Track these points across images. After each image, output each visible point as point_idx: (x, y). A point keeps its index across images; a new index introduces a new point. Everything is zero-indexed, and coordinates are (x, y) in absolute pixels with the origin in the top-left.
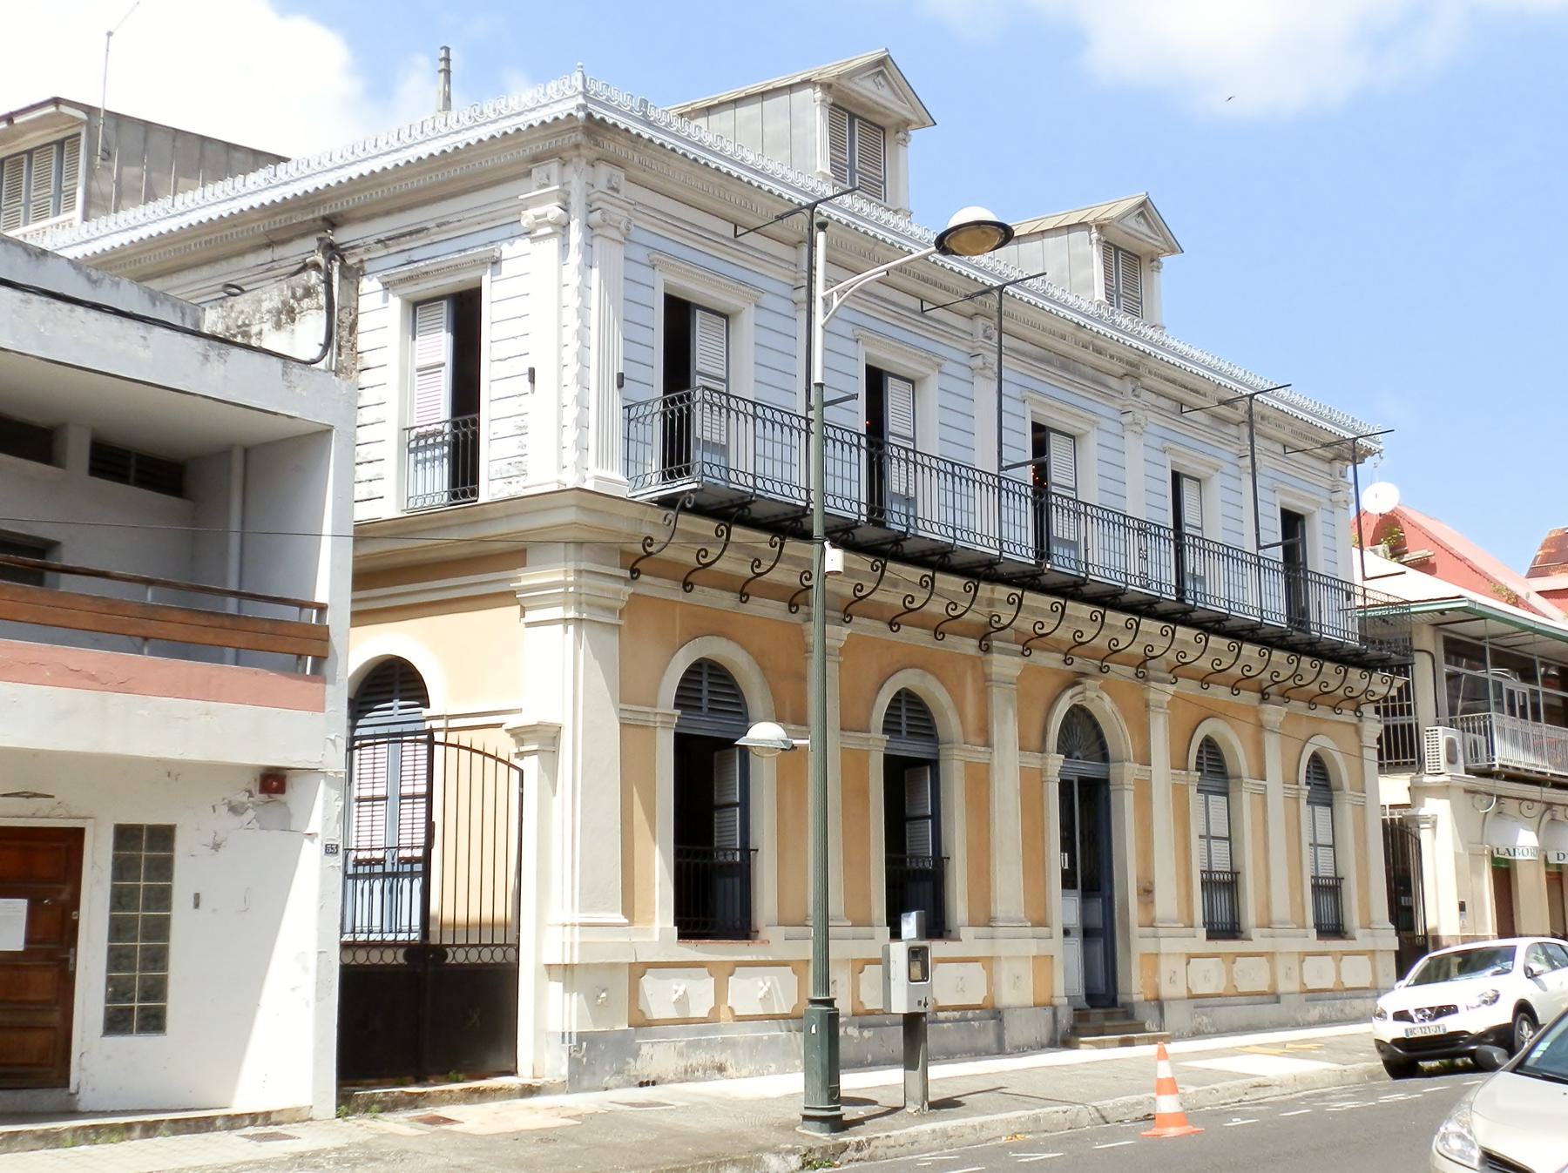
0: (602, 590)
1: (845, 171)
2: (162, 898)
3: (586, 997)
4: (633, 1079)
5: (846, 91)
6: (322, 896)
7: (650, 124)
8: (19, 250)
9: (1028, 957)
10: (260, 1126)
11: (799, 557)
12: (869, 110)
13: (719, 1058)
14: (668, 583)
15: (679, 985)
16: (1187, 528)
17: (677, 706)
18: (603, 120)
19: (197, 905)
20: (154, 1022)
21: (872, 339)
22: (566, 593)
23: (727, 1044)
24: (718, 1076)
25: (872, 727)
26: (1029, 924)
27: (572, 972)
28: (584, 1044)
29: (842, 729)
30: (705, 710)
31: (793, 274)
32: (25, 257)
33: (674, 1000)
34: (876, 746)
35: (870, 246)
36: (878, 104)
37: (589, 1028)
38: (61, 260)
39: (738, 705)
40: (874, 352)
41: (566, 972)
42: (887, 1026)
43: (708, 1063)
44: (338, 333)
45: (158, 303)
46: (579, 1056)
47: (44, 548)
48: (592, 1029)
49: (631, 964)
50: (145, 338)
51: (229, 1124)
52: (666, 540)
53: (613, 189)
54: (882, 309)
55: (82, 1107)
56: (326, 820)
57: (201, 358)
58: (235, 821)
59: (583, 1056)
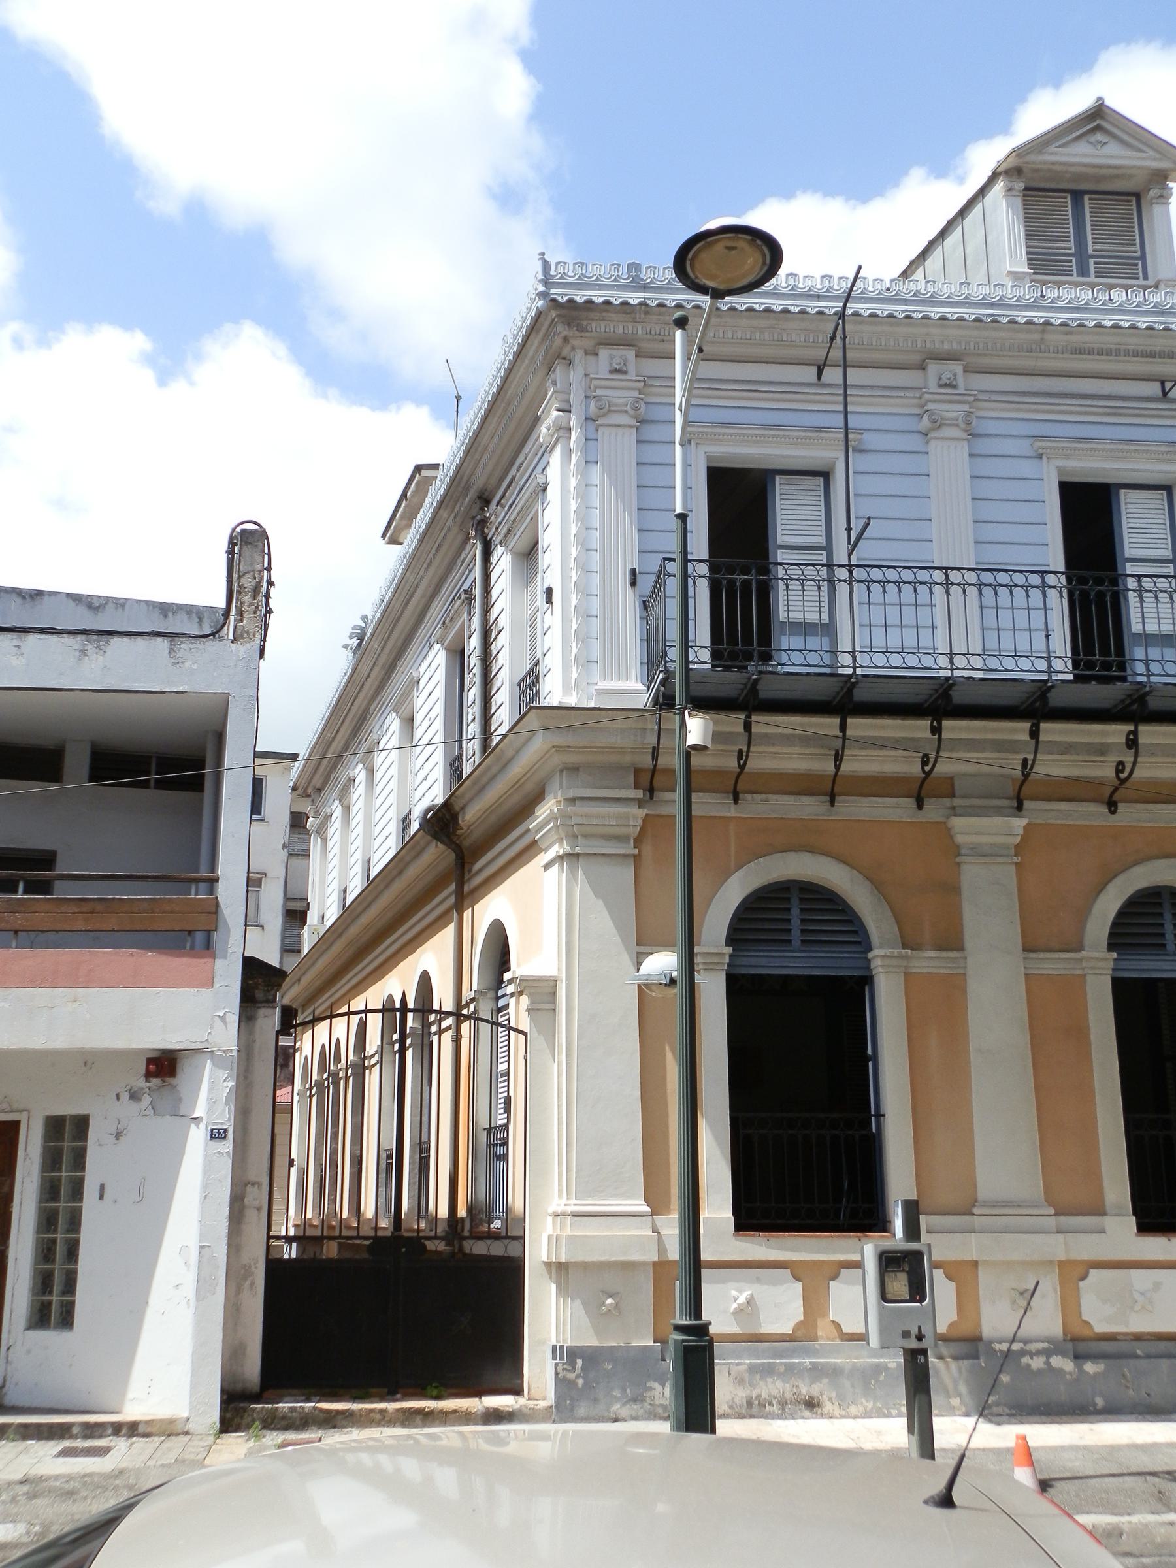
0: (587, 816)
1: (1136, 265)
2: (77, 1191)
3: (585, 1305)
4: (660, 1410)
5: (1045, 167)
6: (206, 1186)
7: (645, 288)
8: (14, 596)
9: (1051, 1262)
10: (123, 1436)
11: (913, 739)
12: (1099, 179)
13: (806, 1389)
14: (1092, 807)
15: (741, 1291)
16: (1128, 565)
17: (727, 944)
18: (571, 301)
19: (101, 1197)
20: (66, 1320)
21: (1063, 448)
22: (556, 827)
23: (817, 1372)
24: (807, 1413)
25: (1088, 940)
26: (1053, 1212)
27: (567, 1269)
28: (579, 1362)
29: (1025, 950)
30: (796, 943)
31: (916, 401)
32: (19, 600)
33: (732, 1310)
34: (1092, 968)
35: (1037, 336)
36: (1100, 167)
37: (591, 1341)
38: (59, 595)
39: (850, 922)
40: (1061, 463)
41: (560, 1270)
42: (1137, 1357)
43: (788, 1396)
44: (237, 599)
45: (170, 614)
46: (572, 1376)
47: (46, 860)
48: (593, 1342)
49: (654, 1263)
50: (18, 647)
51: (88, 1432)
52: (1132, 759)
53: (946, 385)
54: (1078, 409)
55: (11, 1399)
56: (212, 1103)
57: (78, 653)
58: (134, 1107)
59: (578, 1377)
